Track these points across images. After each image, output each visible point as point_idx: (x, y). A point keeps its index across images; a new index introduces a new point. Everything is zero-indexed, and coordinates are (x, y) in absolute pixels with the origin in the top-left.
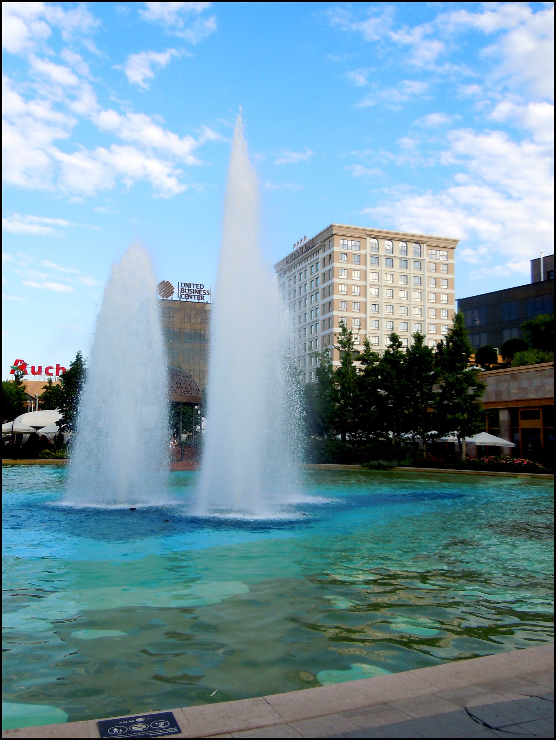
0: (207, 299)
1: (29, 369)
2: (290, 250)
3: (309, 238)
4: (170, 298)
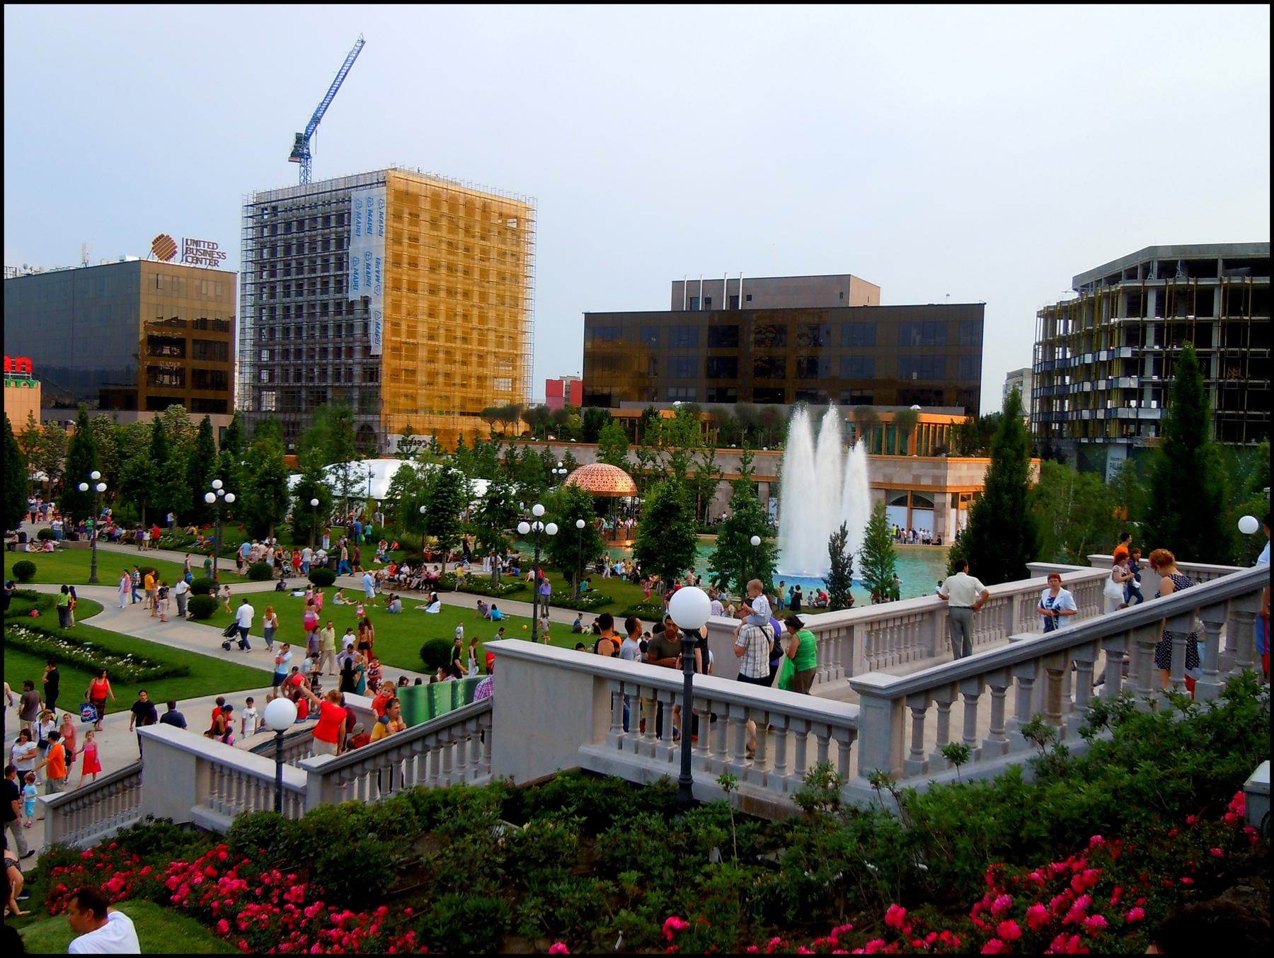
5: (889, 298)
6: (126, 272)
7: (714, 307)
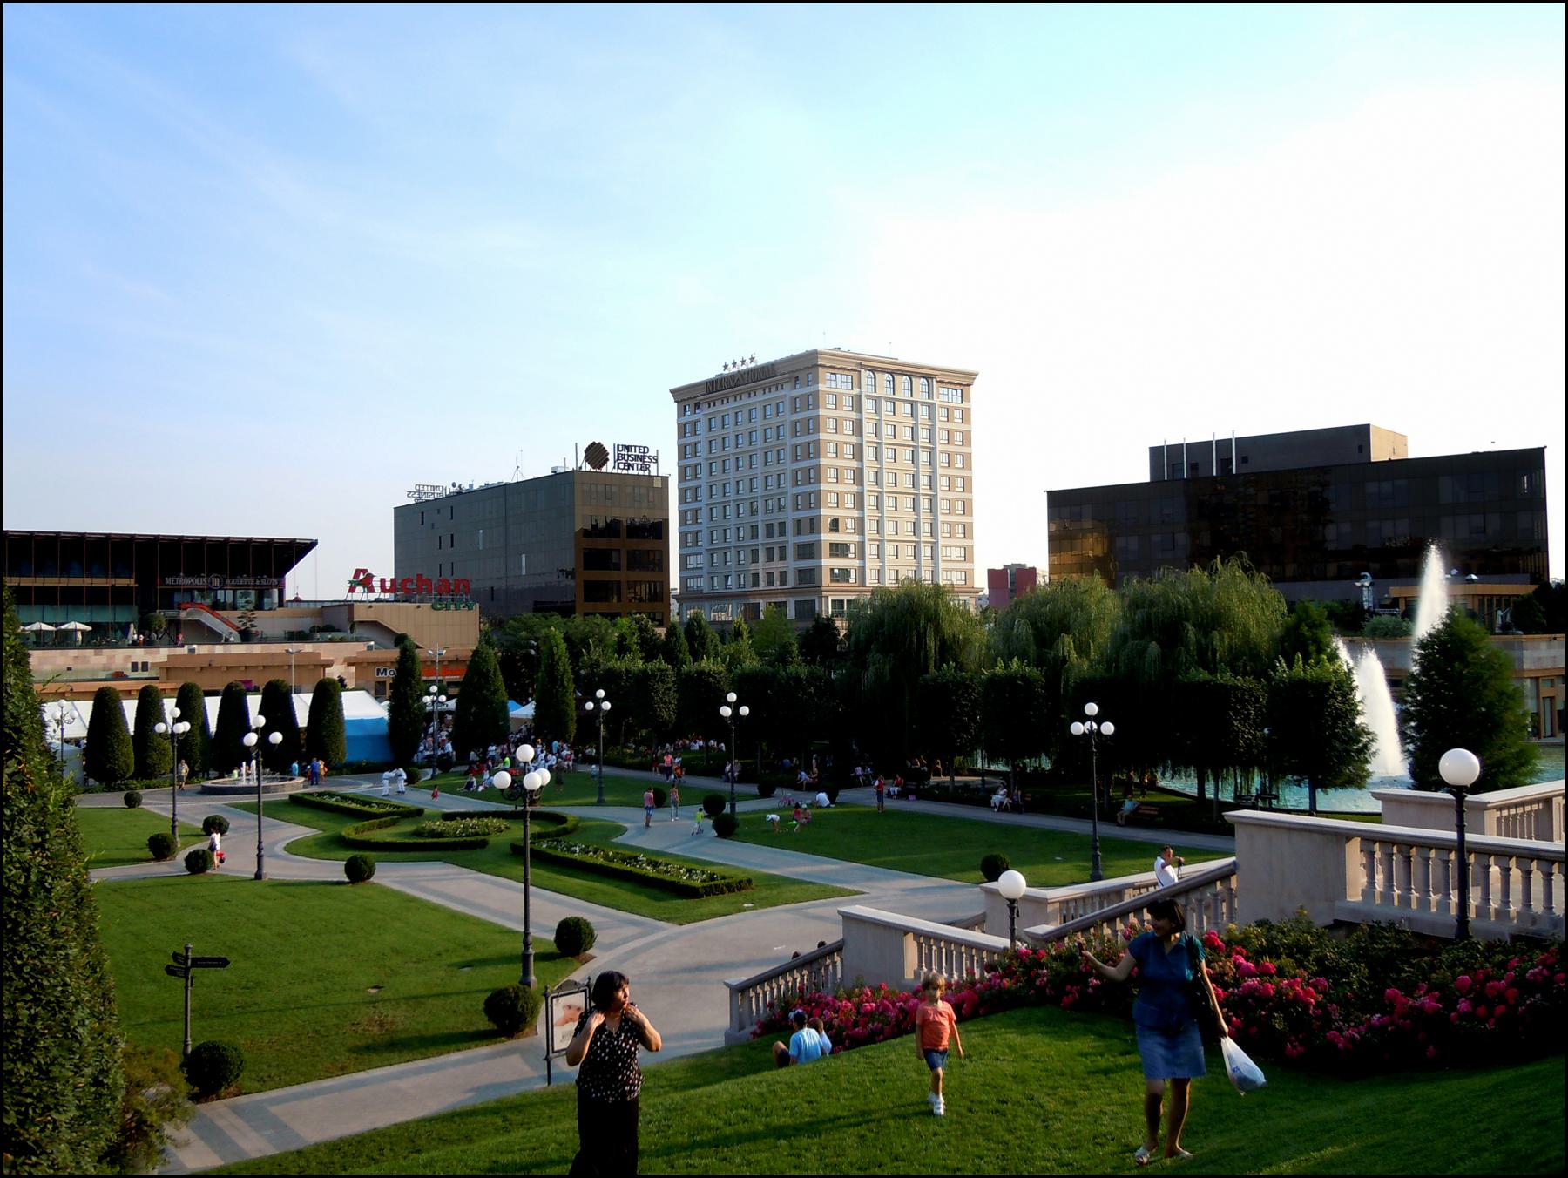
1: (376, 584)
3: (762, 360)
5: (1418, 449)
6: (559, 482)
7: (1202, 473)
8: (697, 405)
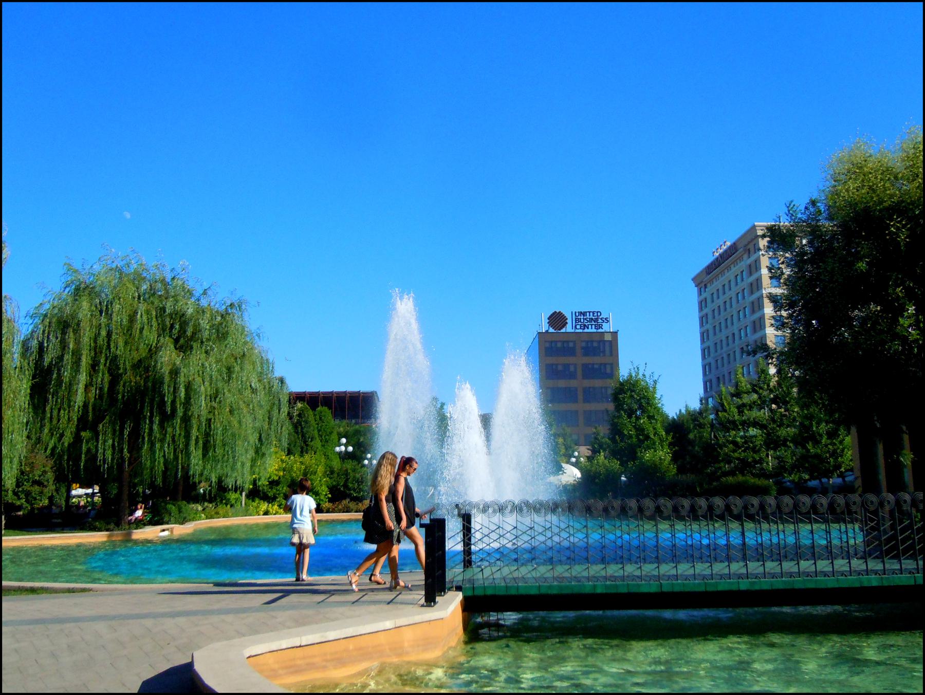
0: (606, 327)
2: (708, 259)
4: (563, 330)
8: (706, 286)
